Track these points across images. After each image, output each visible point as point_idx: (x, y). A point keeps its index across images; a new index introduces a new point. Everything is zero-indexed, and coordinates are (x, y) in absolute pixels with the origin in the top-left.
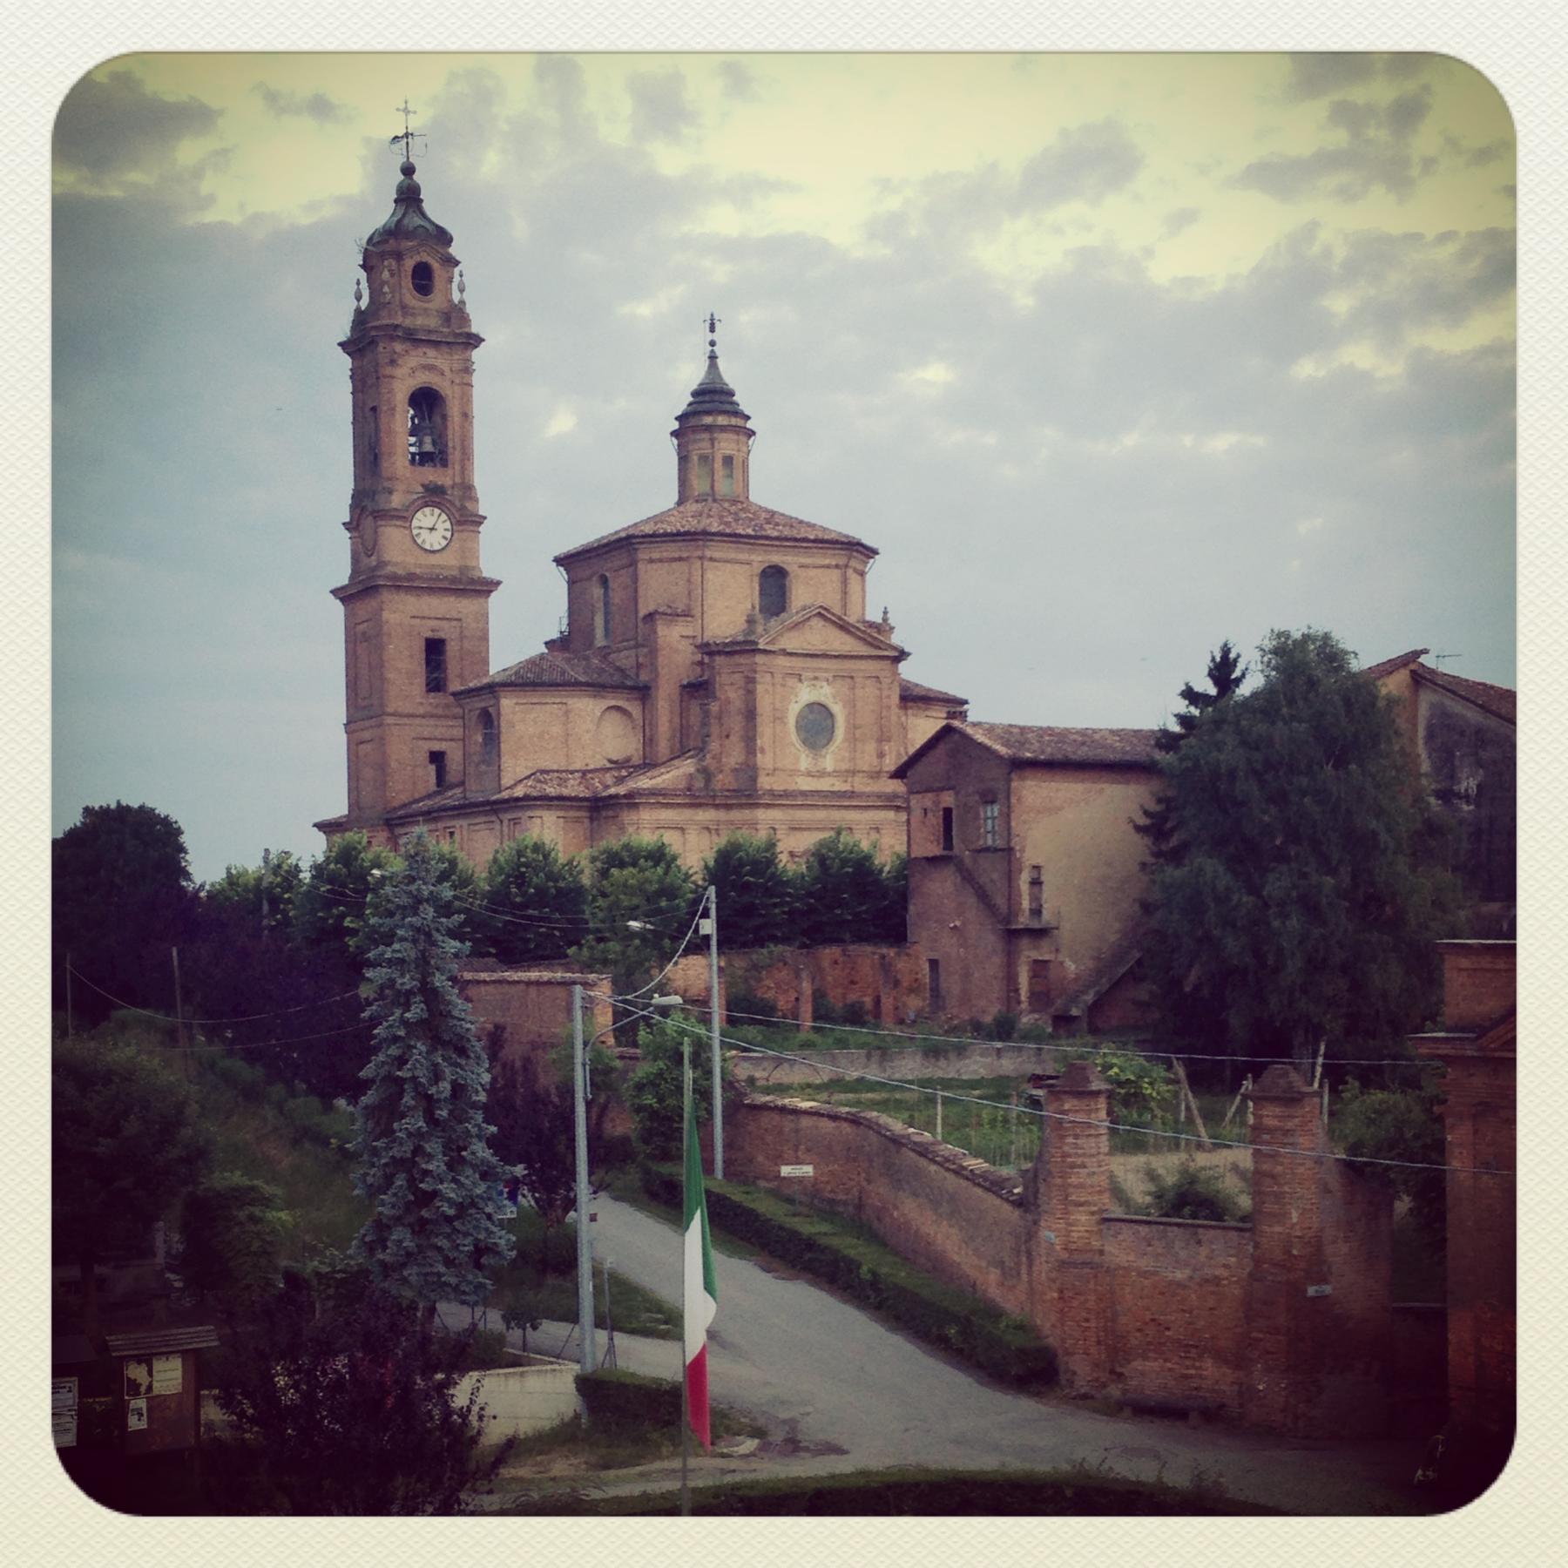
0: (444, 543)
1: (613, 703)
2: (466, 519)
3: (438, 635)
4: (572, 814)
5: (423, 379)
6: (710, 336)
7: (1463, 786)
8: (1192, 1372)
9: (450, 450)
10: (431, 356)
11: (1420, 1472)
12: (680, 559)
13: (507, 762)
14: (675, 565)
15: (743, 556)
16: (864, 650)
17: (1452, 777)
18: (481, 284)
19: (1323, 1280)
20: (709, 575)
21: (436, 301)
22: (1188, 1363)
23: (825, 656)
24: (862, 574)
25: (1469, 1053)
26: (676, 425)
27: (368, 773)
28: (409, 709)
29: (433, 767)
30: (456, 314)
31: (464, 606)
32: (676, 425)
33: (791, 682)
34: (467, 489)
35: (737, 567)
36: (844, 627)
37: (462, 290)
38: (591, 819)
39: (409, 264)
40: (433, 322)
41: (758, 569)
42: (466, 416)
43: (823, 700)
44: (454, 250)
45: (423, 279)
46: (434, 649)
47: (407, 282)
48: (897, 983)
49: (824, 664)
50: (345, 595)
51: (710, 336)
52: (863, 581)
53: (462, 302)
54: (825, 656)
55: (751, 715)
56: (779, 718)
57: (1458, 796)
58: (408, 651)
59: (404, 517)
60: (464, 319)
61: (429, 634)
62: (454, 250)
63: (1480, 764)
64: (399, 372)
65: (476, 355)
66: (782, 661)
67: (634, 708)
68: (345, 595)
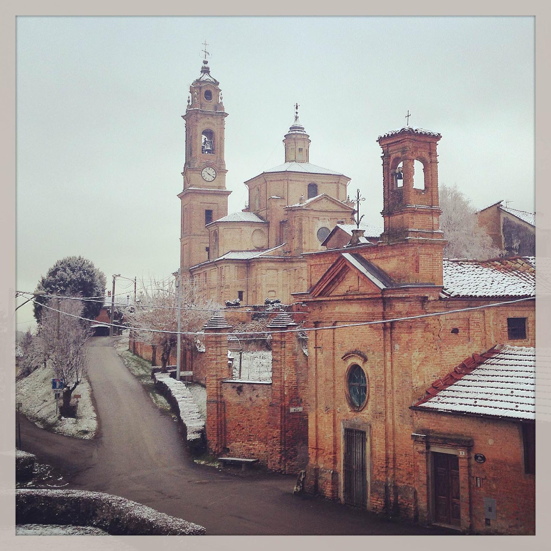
0: (213, 179)
1: (257, 228)
2: (221, 171)
3: (209, 209)
4: (240, 265)
5: (206, 126)
6: (296, 111)
7: (515, 245)
8: (251, 447)
9: (216, 149)
10: (211, 119)
11: (295, 488)
12: (281, 180)
13: (221, 248)
14: (279, 182)
15: (301, 179)
16: (341, 210)
17: (512, 243)
18: (228, 98)
19: (299, 405)
20: (290, 185)
21: (213, 101)
22: (250, 443)
23: (326, 211)
24: (345, 186)
25: (310, 300)
26: (284, 138)
27: (186, 255)
28: (199, 233)
29: (207, 252)
30: (219, 106)
31: (219, 199)
32: (284, 138)
33: (315, 220)
34: (222, 162)
35: (300, 183)
36: (334, 202)
37: (221, 98)
38: (247, 267)
39: (204, 91)
40: (211, 110)
41: (307, 184)
42: (222, 139)
43: (327, 226)
44: (219, 87)
45: (208, 95)
46: (209, 214)
47: (203, 96)
48: (237, 304)
49: (326, 214)
50: (181, 196)
51: (296, 111)
52: (346, 188)
53: (221, 103)
54: (326, 211)
55: (301, 231)
56: (311, 232)
57: (513, 249)
58: (202, 214)
59: (200, 170)
60: (223, 108)
61: (207, 209)
62: (219, 87)
63: (519, 238)
64: (198, 124)
65: (225, 119)
66: (312, 213)
67: (265, 230)
68: (181, 196)
